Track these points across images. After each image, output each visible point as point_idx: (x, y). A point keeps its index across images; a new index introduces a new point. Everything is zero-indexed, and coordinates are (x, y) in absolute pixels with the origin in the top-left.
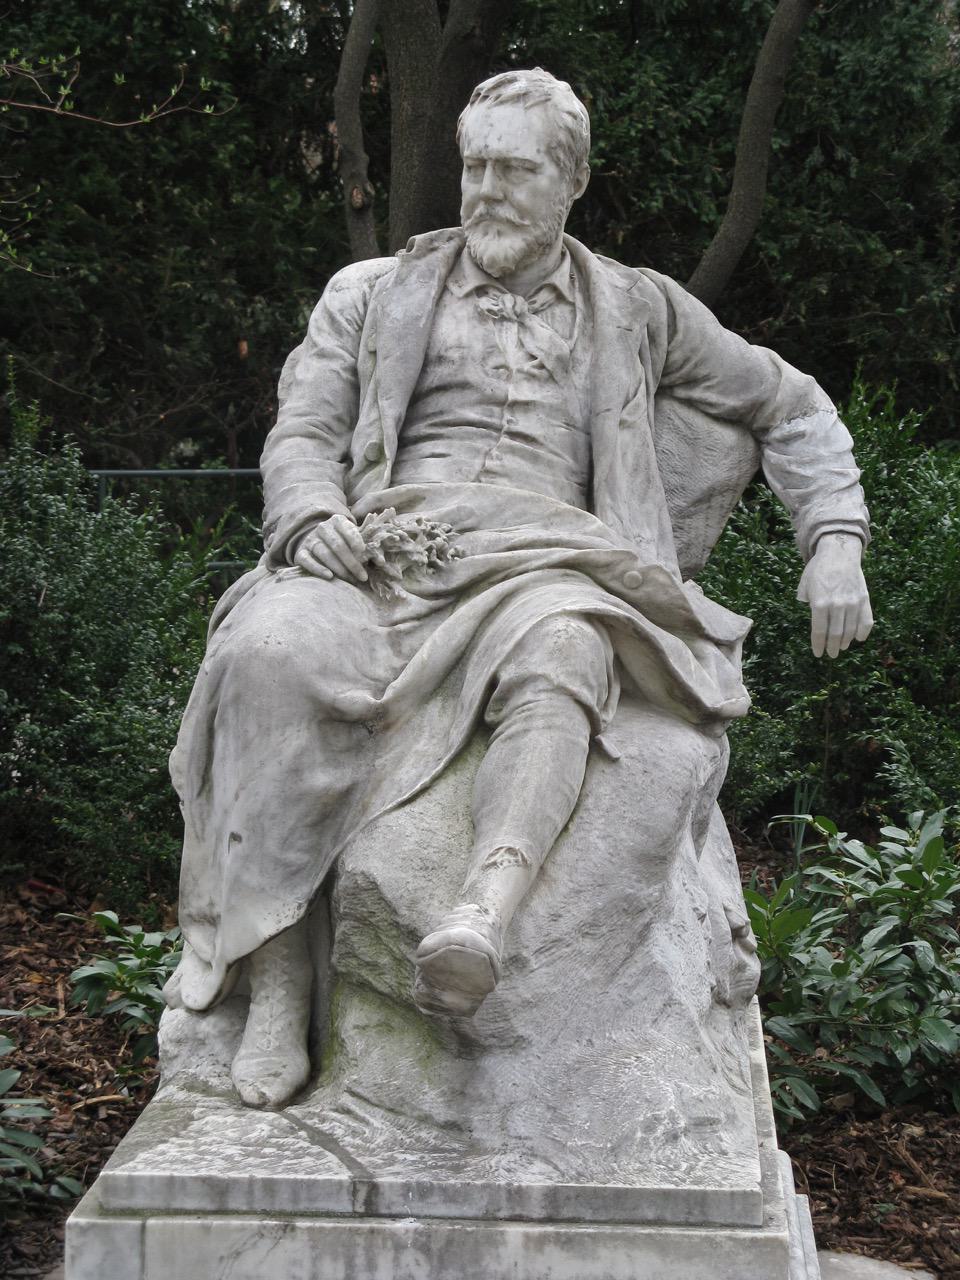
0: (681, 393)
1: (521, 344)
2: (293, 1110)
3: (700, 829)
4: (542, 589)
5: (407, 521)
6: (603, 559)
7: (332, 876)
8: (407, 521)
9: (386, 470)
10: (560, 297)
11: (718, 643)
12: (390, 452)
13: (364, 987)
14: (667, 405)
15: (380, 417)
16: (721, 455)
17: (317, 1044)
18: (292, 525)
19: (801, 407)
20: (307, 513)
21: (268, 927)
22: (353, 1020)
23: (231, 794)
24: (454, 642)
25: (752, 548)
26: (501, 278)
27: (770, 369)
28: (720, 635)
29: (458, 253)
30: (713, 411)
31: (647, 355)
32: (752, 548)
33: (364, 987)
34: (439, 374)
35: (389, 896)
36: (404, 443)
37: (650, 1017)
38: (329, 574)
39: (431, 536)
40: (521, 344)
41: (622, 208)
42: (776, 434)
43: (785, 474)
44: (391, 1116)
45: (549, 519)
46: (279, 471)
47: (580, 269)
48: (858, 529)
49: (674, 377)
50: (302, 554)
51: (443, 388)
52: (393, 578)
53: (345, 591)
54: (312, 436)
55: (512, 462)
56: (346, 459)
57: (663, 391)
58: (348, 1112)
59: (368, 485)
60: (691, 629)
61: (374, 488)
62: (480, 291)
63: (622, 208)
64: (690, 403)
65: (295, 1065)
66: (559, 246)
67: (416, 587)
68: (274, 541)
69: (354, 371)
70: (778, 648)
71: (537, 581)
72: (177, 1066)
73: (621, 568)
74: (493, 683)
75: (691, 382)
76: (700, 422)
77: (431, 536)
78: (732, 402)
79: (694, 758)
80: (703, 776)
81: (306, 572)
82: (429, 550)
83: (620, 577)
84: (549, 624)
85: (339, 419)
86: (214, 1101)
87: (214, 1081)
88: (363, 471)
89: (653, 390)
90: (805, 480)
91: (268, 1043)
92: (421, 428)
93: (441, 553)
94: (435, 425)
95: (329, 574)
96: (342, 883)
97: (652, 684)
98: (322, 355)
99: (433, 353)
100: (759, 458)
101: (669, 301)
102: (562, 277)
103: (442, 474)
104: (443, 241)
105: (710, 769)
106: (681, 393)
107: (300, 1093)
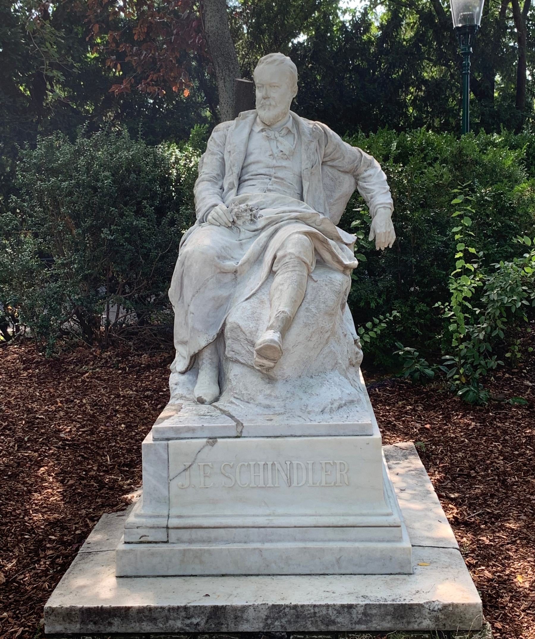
0: (329, 163)
1: (277, 147)
2: (215, 404)
3: (343, 307)
4: (289, 226)
5: (243, 206)
6: (307, 216)
7: (224, 324)
8: (243, 206)
9: (234, 191)
10: (290, 131)
11: (346, 244)
12: (236, 185)
13: (237, 361)
14: (326, 168)
15: (231, 178)
16: (347, 187)
17: (221, 380)
18: (206, 208)
19: (370, 165)
20: (208, 206)
21: (203, 344)
22: (234, 372)
23: (190, 299)
24: (261, 245)
25: (354, 215)
26: (268, 126)
27: (359, 154)
28: (353, 180)
29: (255, 119)
30: (341, 169)
31: (318, 151)
32: (354, 215)
33: (237, 361)
34: (251, 159)
35: (244, 330)
36: (241, 181)
37: (330, 367)
38: (218, 224)
39: (251, 210)
40: (277, 147)
41: (306, 104)
42: (362, 176)
43: (364, 189)
44: (222, 270)
45: (288, 205)
46: (201, 192)
47: (296, 123)
48: (389, 206)
49: (327, 159)
50: (209, 217)
51: (254, 163)
52: (240, 225)
53: (222, 229)
54: (209, 181)
55: (275, 186)
56: (222, 188)
57: (323, 163)
58: (234, 403)
59: (229, 196)
60: (339, 239)
61: (232, 196)
62: (262, 130)
63: (306, 104)
64: (332, 167)
65: (215, 389)
66: (289, 114)
67: (246, 228)
68: (199, 216)
69: (223, 159)
70: (366, 251)
71: (288, 223)
72: (176, 392)
73: (314, 219)
74: (275, 258)
75: (333, 160)
76: (336, 173)
77: (251, 210)
78: (348, 167)
79: (342, 282)
80: (345, 288)
81: (211, 224)
82: (251, 215)
83: (314, 222)
84: (291, 239)
85: (218, 175)
86: (188, 402)
87: (188, 396)
88: (228, 191)
89: (321, 163)
90: (373, 190)
91: (205, 385)
92: (246, 177)
93: (255, 217)
94: (252, 175)
95: (218, 224)
96: (228, 326)
97: (327, 256)
98: (213, 154)
99: (249, 152)
100: (357, 184)
101: (325, 132)
102: (290, 124)
103: (253, 193)
104: (249, 114)
105: (346, 286)
106: (329, 163)
107: (217, 400)
